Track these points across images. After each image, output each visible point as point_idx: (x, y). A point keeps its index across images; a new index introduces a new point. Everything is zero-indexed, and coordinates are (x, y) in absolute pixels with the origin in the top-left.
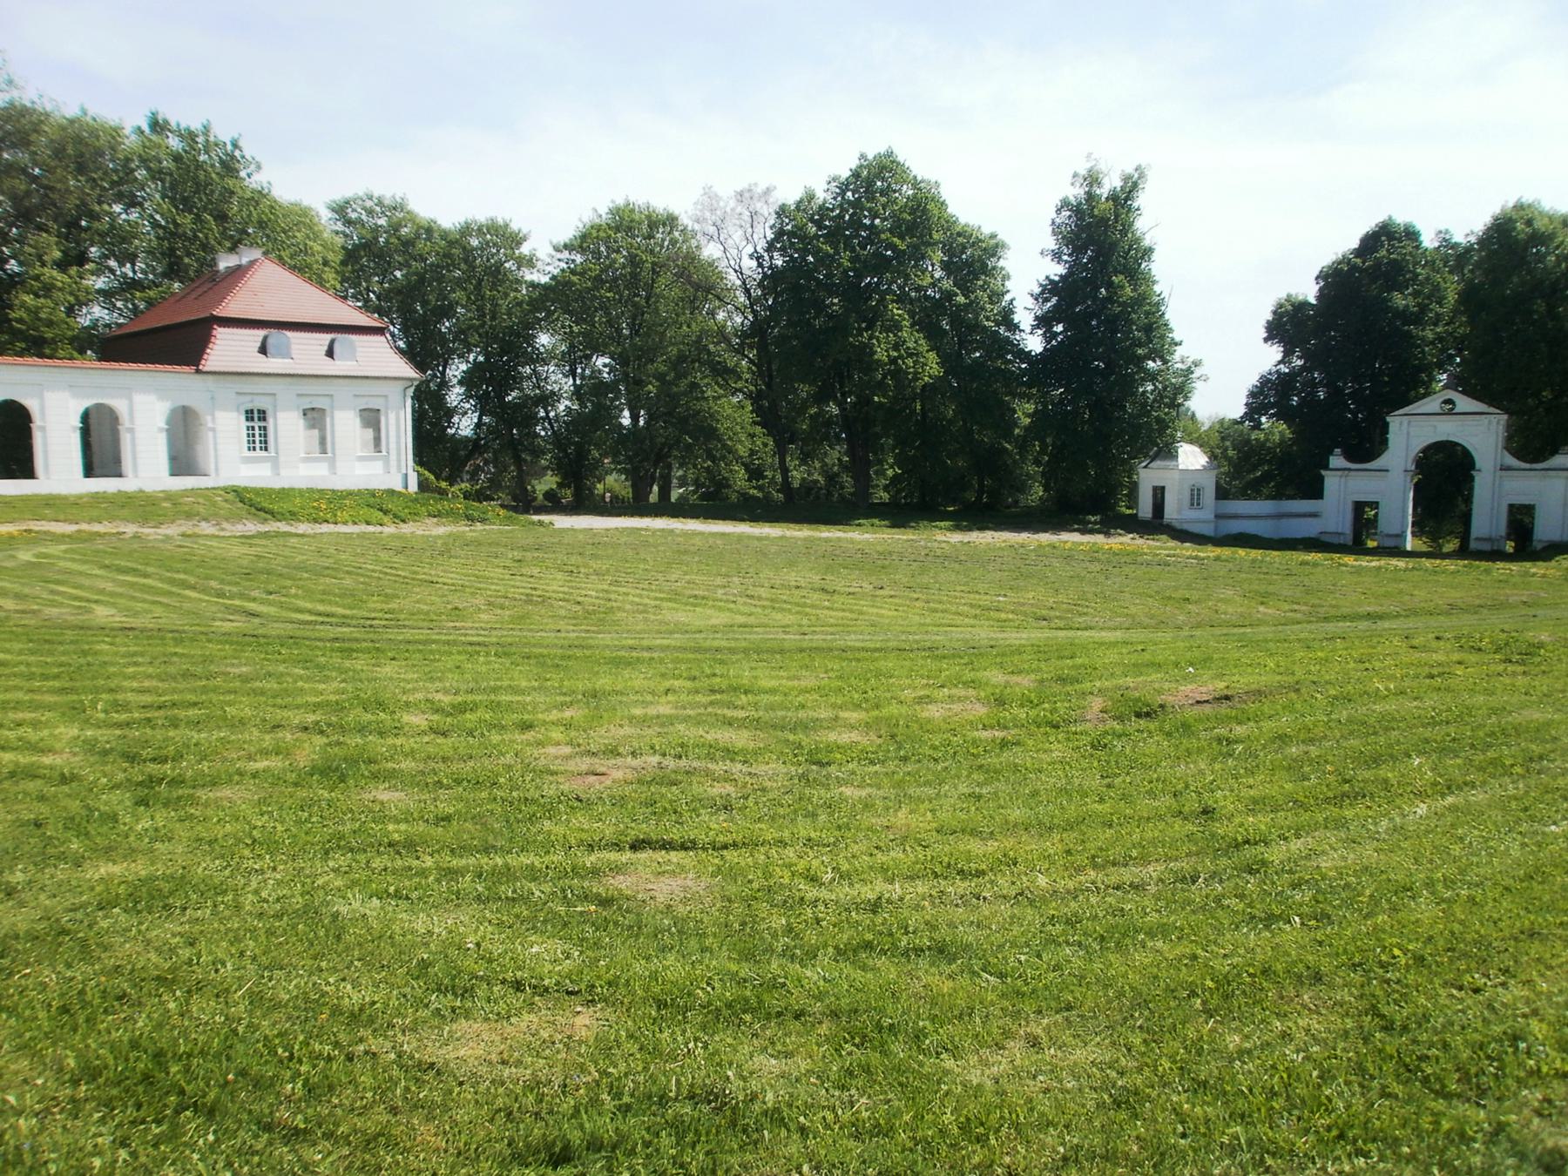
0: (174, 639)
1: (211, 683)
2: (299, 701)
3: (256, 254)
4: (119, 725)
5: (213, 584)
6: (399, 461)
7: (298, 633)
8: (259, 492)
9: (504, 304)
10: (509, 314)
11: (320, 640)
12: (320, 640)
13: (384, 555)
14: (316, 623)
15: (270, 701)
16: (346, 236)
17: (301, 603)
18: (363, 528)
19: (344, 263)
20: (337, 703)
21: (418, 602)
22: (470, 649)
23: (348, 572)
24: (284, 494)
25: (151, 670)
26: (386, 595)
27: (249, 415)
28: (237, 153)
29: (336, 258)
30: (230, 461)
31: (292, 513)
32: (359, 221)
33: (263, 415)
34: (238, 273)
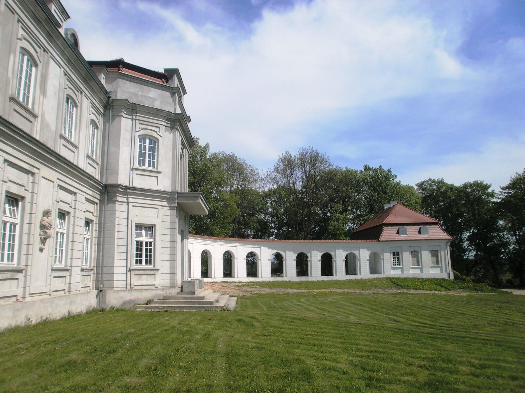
0: (373, 328)
1: (387, 345)
2: (418, 355)
3: (395, 203)
4: (360, 357)
5: (384, 310)
6: (446, 268)
7: (414, 330)
8: (397, 279)
9: (483, 211)
10: (486, 214)
11: (423, 333)
12: (423, 333)
13: (443, 302)
14: (420, 326)
15: (407, 355)
16: (423, 194)
17: (415, 319)
18: (434, 292)
19: (422, 202)
20: (432, 358)
21: (459, 321)
22: (483, 341)
23: (431, 308)
24: (406, 279)
25: (367, 339)
26: (446, 318)
27: (394, 254)
28: (390, 174)
29: (419, 201)
30: (389, 270)
31: (408, 286)
32: (426, 188)
33: (398, 254)
34: (390, 209)
